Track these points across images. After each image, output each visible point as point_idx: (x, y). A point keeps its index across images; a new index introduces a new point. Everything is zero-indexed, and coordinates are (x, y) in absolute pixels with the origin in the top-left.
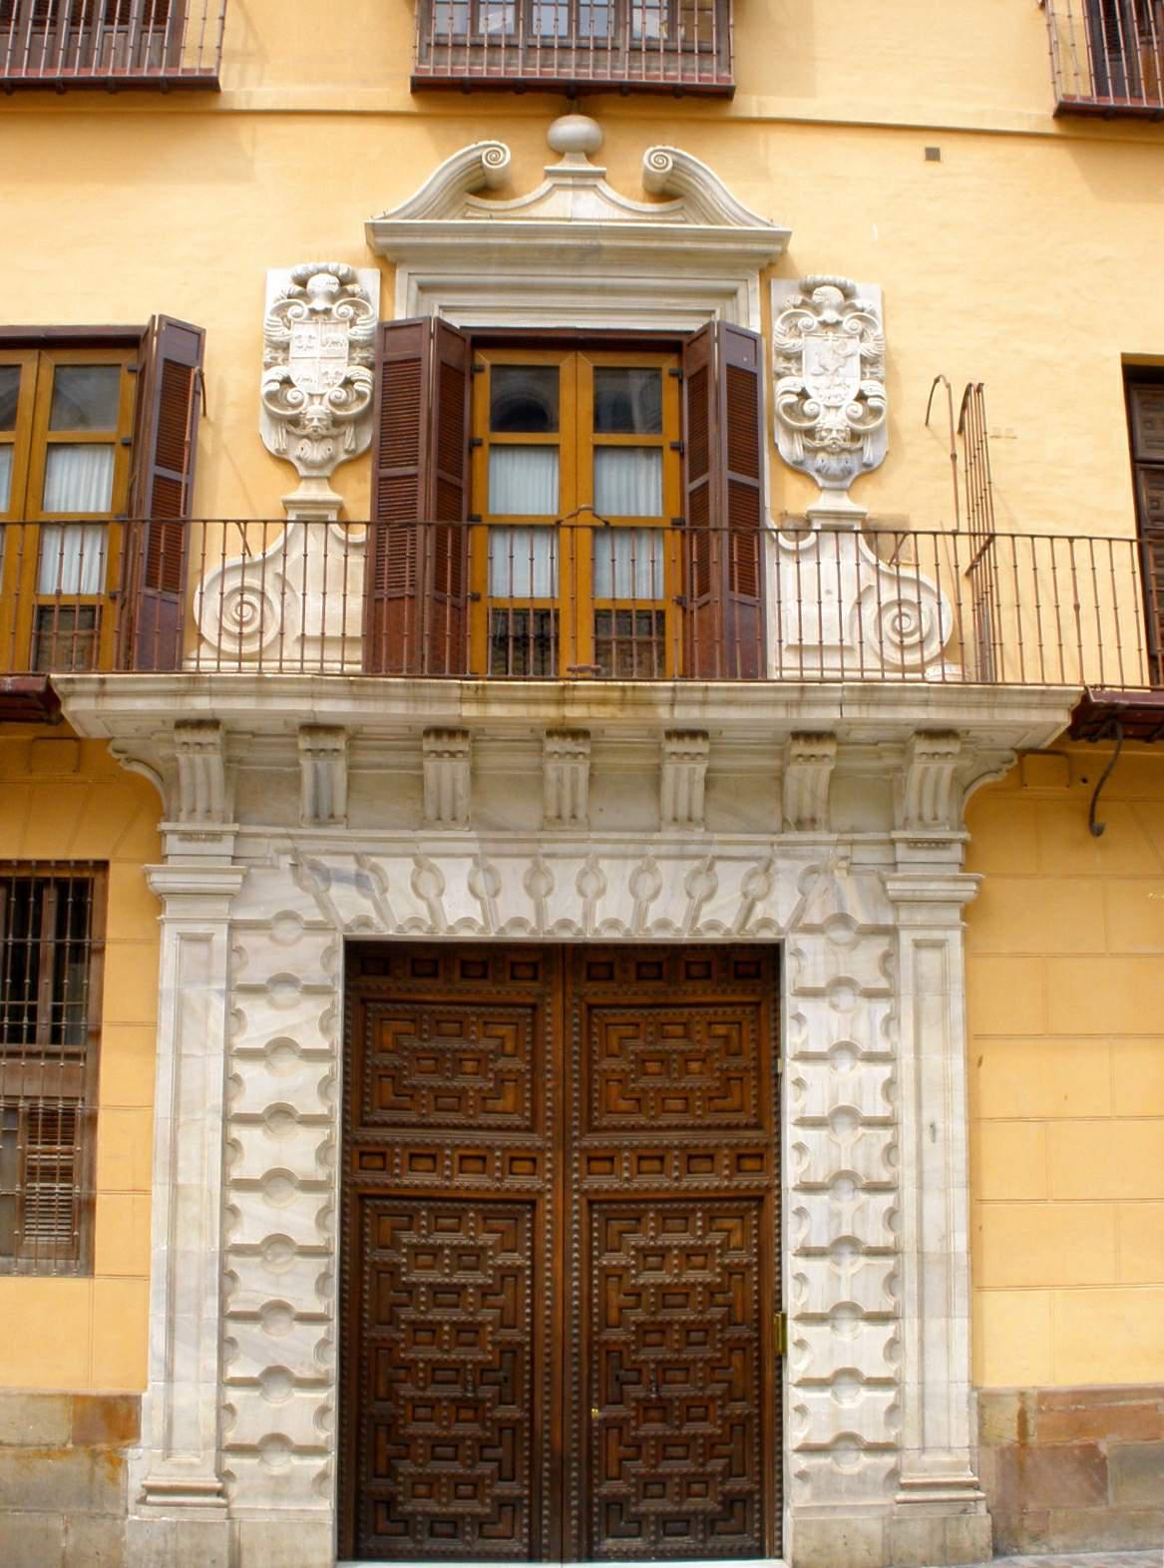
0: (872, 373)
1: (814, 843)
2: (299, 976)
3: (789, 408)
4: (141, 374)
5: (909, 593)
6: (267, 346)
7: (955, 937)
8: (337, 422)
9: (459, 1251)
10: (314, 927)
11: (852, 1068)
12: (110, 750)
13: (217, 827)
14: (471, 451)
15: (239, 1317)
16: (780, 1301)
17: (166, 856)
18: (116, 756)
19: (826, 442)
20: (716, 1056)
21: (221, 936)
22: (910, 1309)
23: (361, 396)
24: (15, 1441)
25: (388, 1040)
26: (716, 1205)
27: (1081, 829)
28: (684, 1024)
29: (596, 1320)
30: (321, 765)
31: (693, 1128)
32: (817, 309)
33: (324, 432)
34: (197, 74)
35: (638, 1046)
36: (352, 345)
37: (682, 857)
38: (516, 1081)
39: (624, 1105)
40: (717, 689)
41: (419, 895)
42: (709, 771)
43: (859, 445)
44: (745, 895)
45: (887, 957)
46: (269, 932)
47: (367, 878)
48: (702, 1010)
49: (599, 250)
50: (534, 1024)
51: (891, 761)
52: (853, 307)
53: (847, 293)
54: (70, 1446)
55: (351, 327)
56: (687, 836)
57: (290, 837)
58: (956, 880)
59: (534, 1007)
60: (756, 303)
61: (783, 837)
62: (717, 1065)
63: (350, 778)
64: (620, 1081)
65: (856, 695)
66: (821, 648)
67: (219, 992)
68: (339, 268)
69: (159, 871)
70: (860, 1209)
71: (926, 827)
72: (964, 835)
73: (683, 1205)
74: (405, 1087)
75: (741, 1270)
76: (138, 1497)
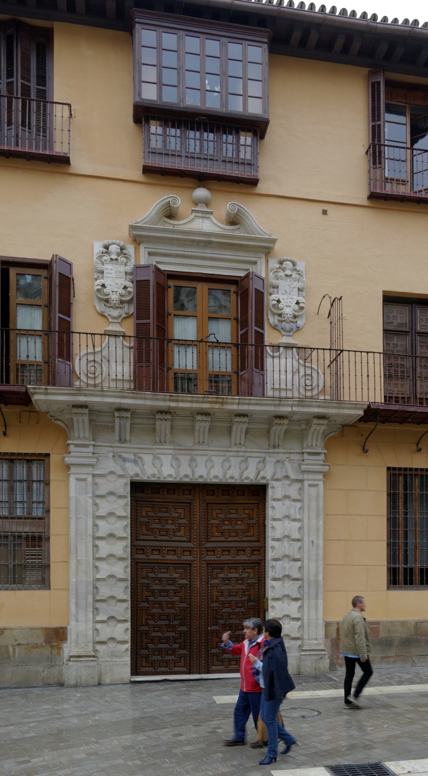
0: (301, 295)
1: (278, 453)
2: (116, 492)
3: (274, 305)
4: (50, 279)
5: (308, 371)
6: (95, 272)
7: (321, 484)
8: (122, 302)
9: (167, 579)
10: (121, 476)
11: (289, 523)
12: (48, 416)
13: (87, 442)
14: (167, 371)
15: (98, 601)
16: (265, 594)
17: (70, 452)
18: (50, 418)
19: (286, 318)
20: (246, 519)
21: (90, 479)
22: (305, 597)
23: (130, 293)
24: (25, 643)
25: (144, 514)
26: (245, 565)
27: (360, 450)
28: (236, 509)
29: (209, 600)
30: (122, 422)
31: (238, 541)
32: (284, 270)
33: (118, 306)
34: (61, 155)
35: (222, 516)
36: (126, 273)
37: (237, 456)
38: (184, 527)
39: (217, 534)
40: (253, 399)
41: (155, 467)
42: (247, 429)
43: (296, 320)
44: (257, 469)
45: (300, 489)
46: (105, 478)
47: (137, 461)
48: (242, 505)
49: (211, 242)
50: (190, 509)
51: (303, 427)
52: (295, 270)
53: (294, 264)
54: (44, 644)
55: (125, 266)
56: (239, 449)
57: (111, 447)
58: (322, 465)
59: (190, 503)
60: (264, 267)
61: (269, 451)
62: (246, 522)
63: (131, 428)
64: (216, 527)
65: (297, 403)
66: (280, 389)
67: (90, 497)
68: (120, 243)
69: (68, 457)
70: (291, 566)
71: (314, 448)
72: (325, 451)
73: (236, 565)
74: (150, 528)
75: (253, 585)
76: (67, 659)
